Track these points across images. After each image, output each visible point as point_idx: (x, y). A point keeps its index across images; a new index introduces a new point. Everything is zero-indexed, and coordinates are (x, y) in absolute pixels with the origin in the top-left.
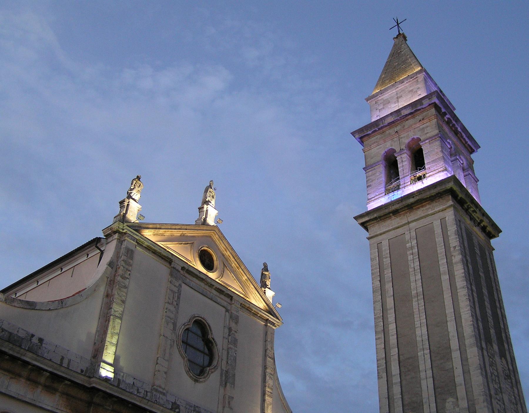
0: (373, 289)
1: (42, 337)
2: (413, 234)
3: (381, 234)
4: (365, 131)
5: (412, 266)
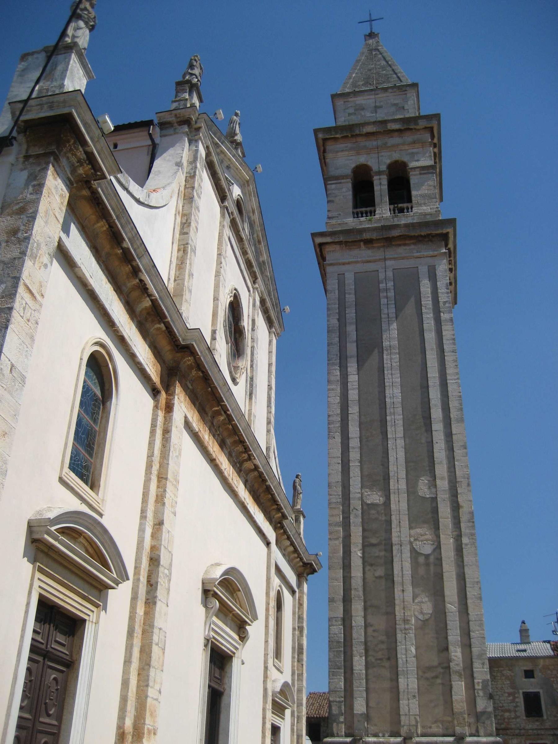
0: (328, 328)
1: (159, 733)
2: (390, 274)
3: (344, 264)
4: (333, 133)
5: (386, 311)
